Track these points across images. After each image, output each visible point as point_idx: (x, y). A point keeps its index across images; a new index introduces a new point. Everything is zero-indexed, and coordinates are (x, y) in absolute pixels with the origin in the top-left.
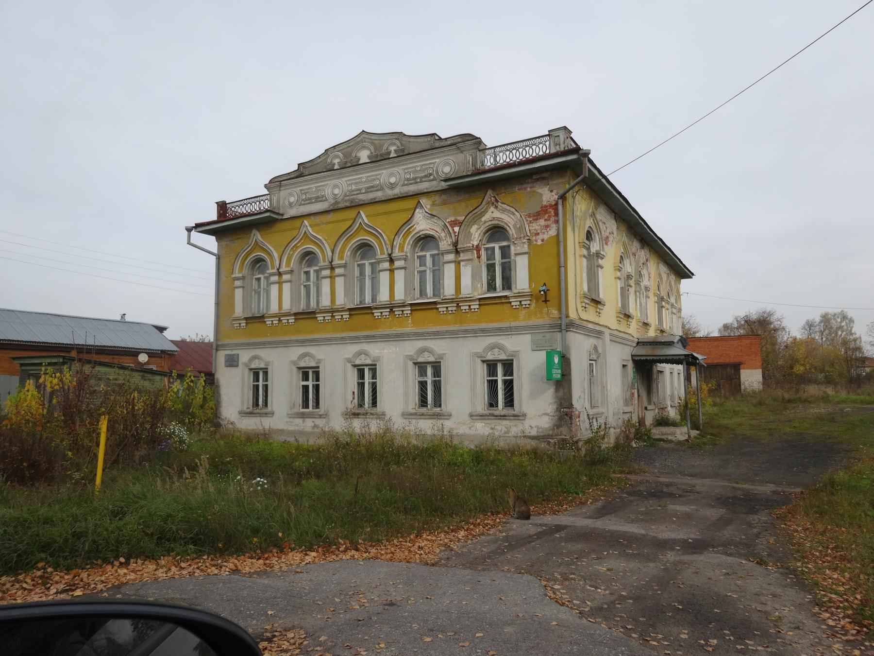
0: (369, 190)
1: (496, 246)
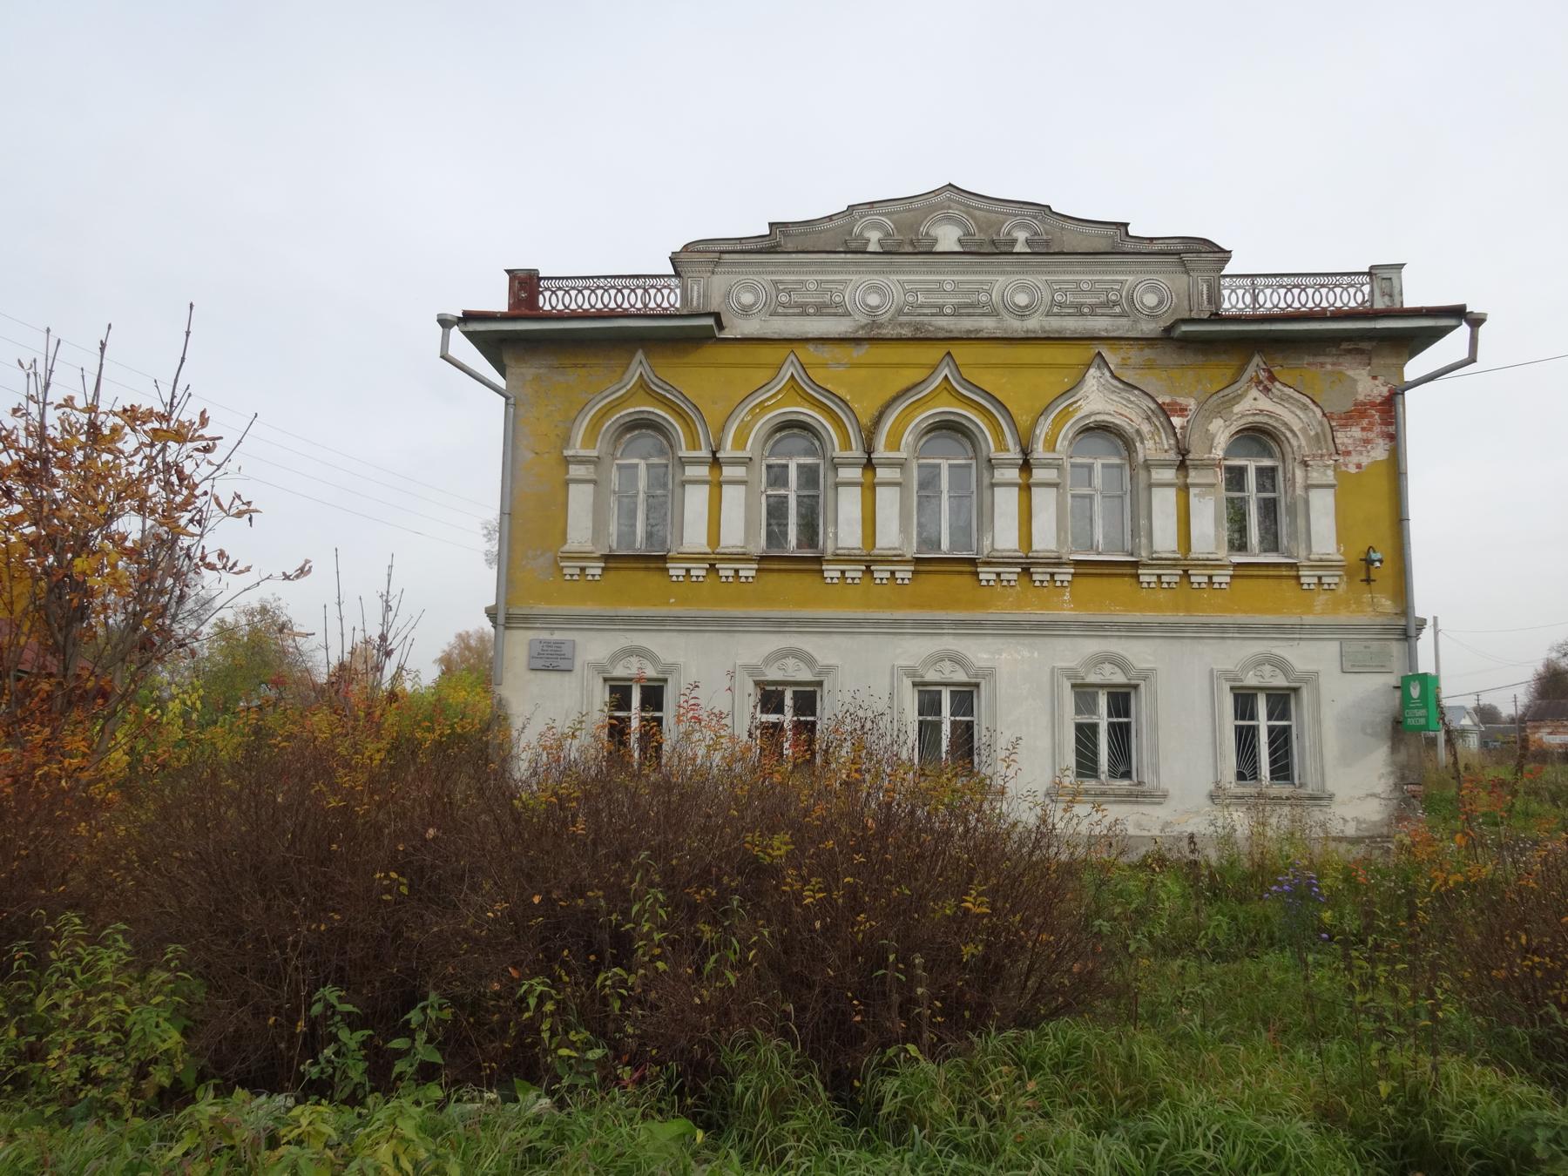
0: (958, 311)
1: (1251, 465)
